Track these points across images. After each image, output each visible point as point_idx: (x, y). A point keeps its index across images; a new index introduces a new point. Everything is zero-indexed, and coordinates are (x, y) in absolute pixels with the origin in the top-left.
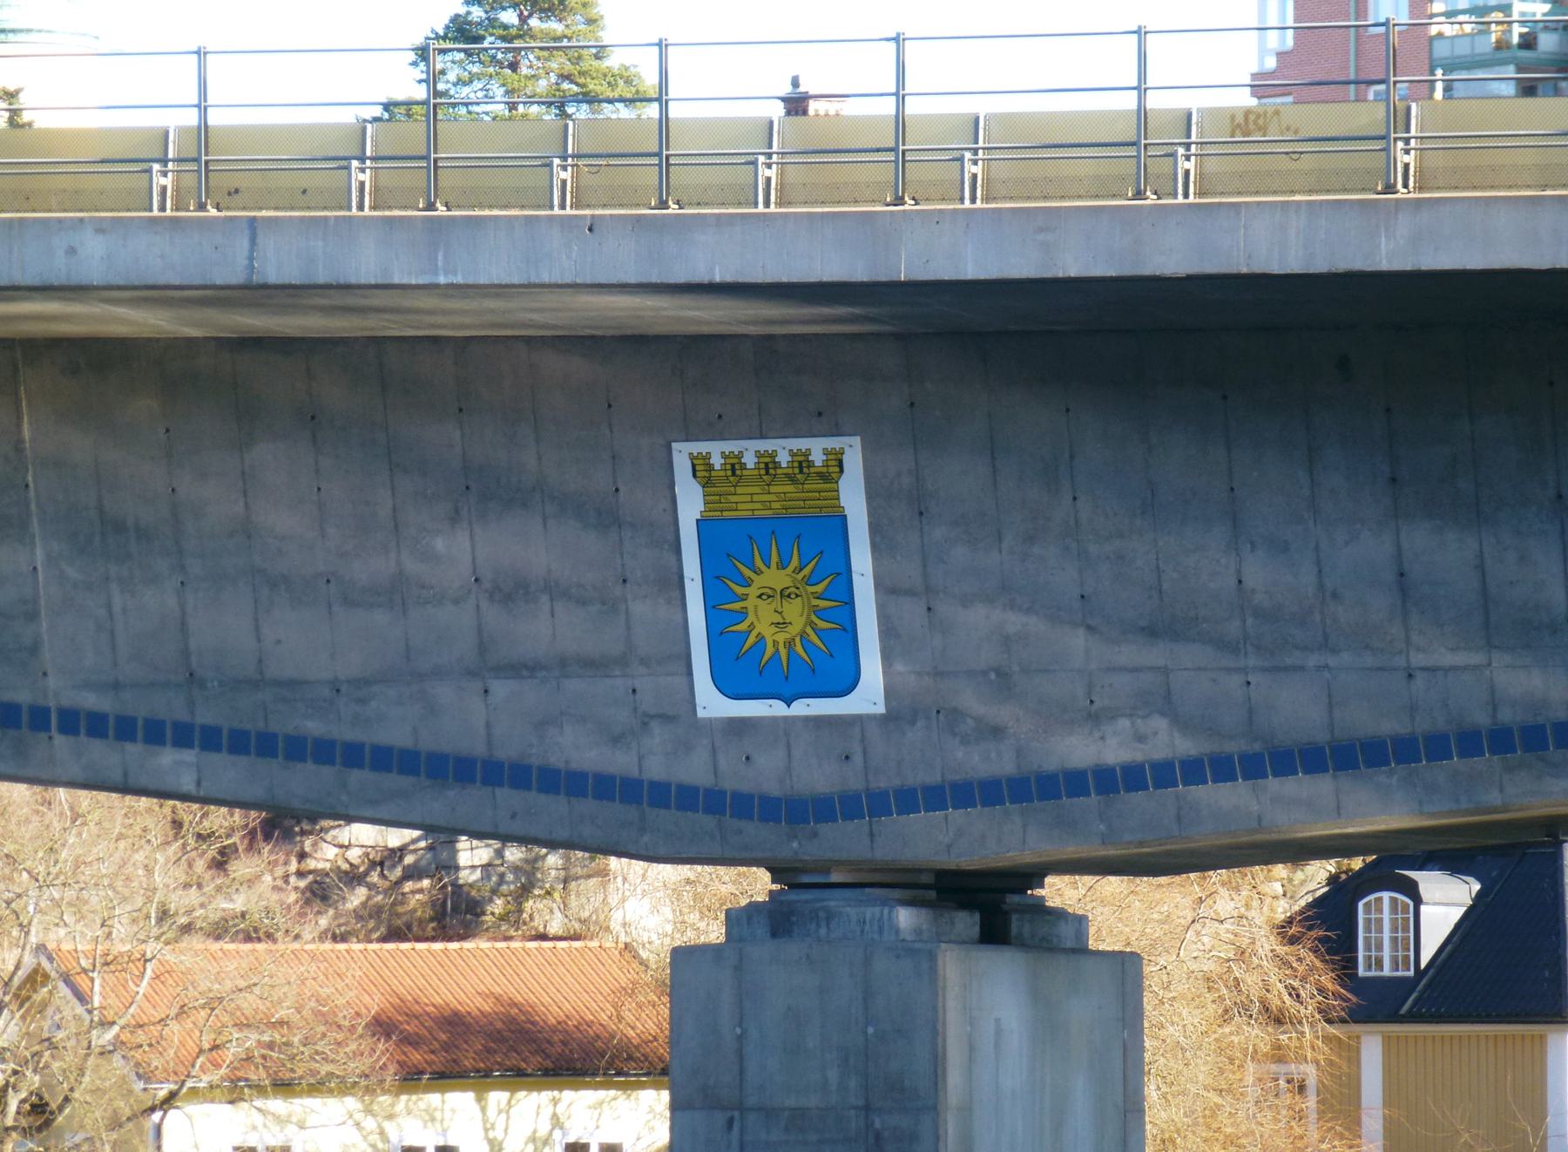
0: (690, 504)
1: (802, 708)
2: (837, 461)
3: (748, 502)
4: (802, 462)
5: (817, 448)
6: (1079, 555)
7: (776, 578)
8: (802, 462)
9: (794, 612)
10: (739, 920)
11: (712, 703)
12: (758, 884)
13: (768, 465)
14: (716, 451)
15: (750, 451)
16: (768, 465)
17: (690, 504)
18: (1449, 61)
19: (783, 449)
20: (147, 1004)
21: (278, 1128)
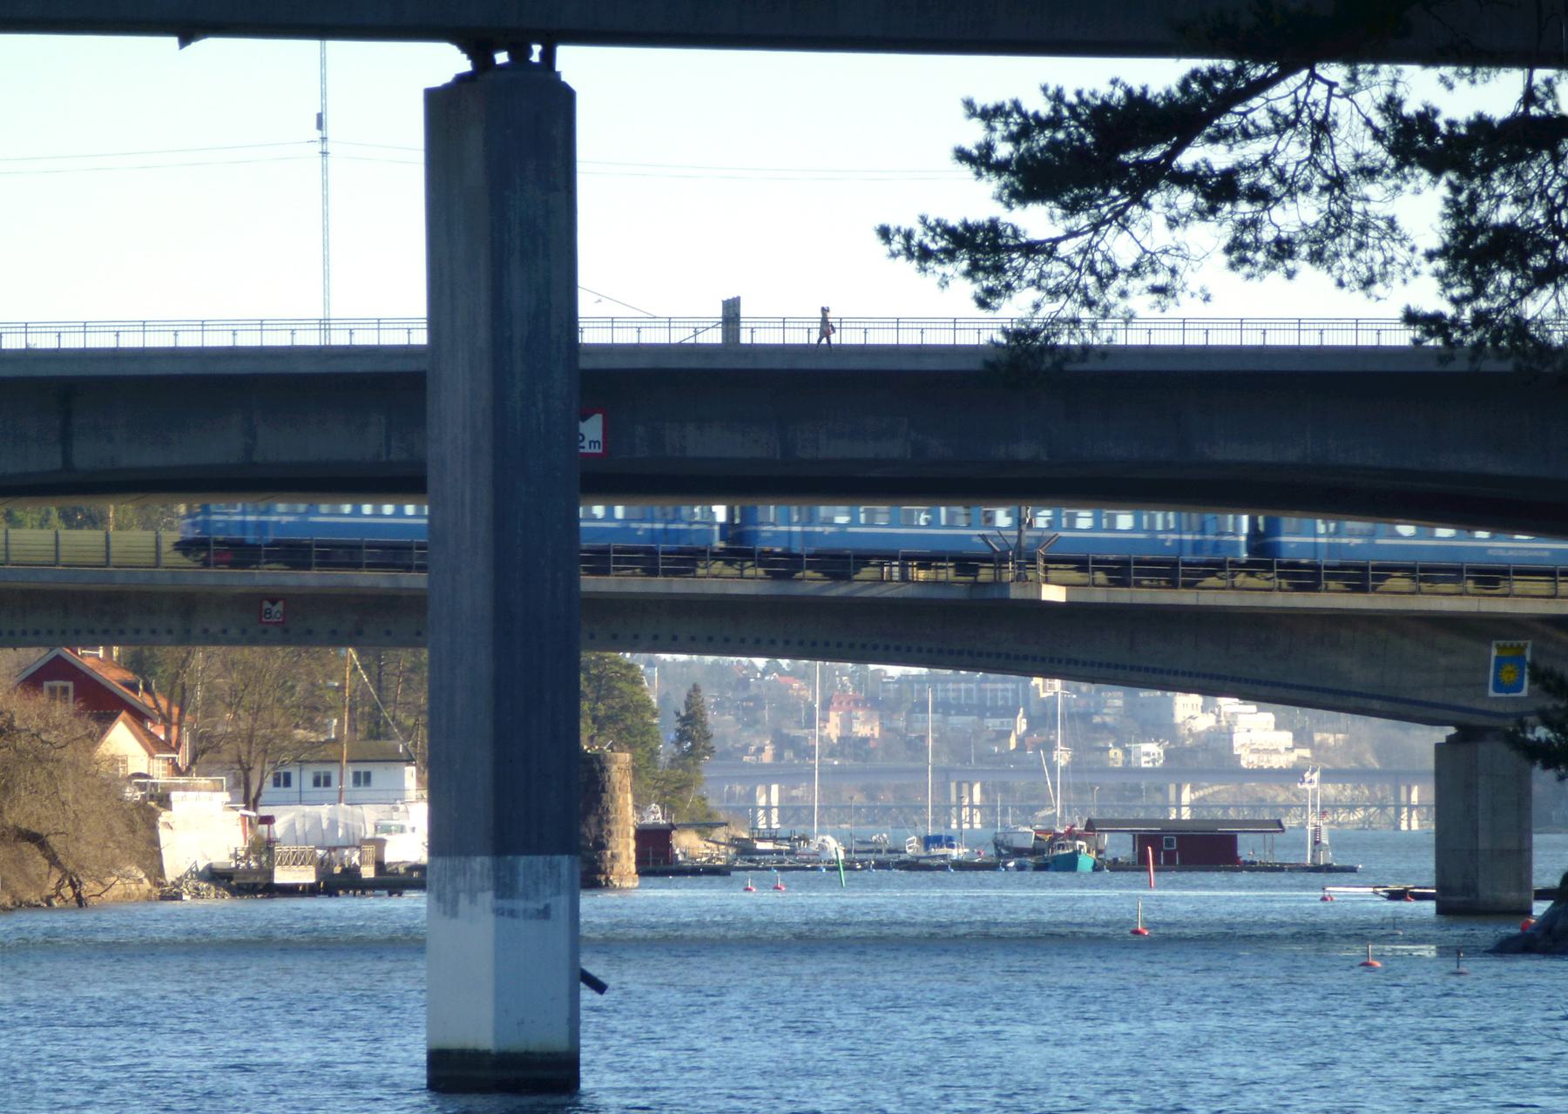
0: (1494, 653)
1: (1510, 695)
2: (1526, 645)
3: (1506, 654)
4: (1519, 646)
5: (1522, 643)
6: (376, 1040)
7: (1509, 668)
8: (1519, 646)
9: (1512, 676)
10: (1450, 738)
11: (1492, 693)
12: (1451, 730)
13: (1512, 646)
14: (1501, 642)
15: (1508, 643)
16: (1512, 646)
17: (1494, 653)
18: (1021, 930)
19: (1515, 643)
20: (946, 1077)
21: (1288, 168)
